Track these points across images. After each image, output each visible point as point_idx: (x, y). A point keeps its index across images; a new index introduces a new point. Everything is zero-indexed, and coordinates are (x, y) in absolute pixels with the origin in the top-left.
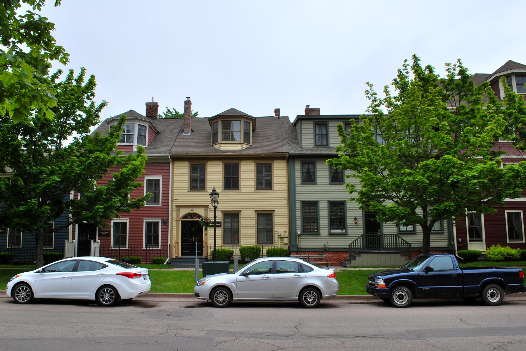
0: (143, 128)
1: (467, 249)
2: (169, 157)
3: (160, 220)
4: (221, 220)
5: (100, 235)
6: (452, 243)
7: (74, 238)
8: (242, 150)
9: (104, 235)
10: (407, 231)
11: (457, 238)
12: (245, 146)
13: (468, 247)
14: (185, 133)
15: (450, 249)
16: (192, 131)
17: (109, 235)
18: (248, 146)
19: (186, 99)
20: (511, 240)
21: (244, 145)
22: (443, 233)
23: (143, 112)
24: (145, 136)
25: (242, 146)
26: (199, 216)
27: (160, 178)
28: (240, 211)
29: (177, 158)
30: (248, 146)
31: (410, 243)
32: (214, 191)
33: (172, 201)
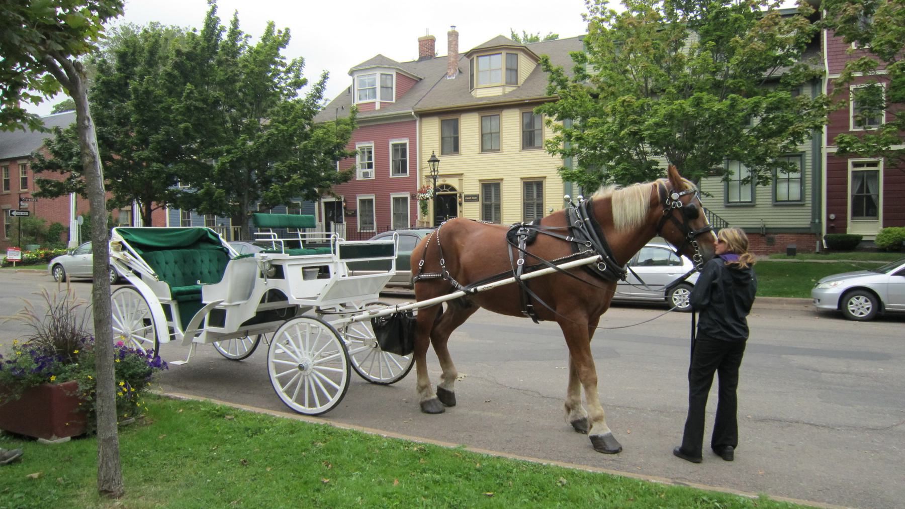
0: (389, 77)
1: (845, 231)
2: (413, 113)
3: (407, 195)
4: (478, 193)
5: (346, 215)
6: (817, 221)
7: (320, 220)
8: (505, 95)
9: (350, 216)
10: (740, 202)
11: (828, 213)
12: (509, 89)
13: (849, 228)
14: (450, 77)
15: (813, 231)
16: (460, 72)
17: (354, 215)
18: (514, 88)
19: (450, 30)
20: (855, 218)
21: (507, 88)
22: (803, 205)
23: (302, 78)
24: (392, 88)
25: (504, 90)
26: (453, 189)
27: (406, 141)
28: (502, 179)
29: (424, 115)
30: (514, 88)
31: (727, 220)
32: (433, 156)
33: (421, 170)
